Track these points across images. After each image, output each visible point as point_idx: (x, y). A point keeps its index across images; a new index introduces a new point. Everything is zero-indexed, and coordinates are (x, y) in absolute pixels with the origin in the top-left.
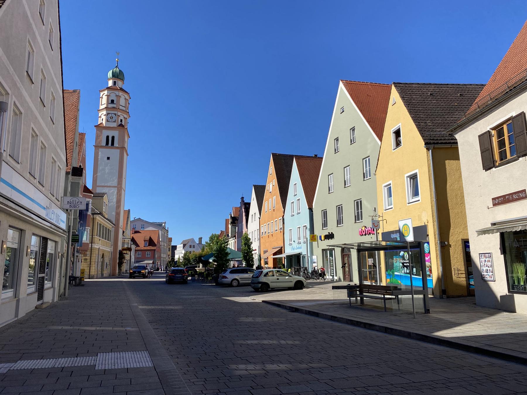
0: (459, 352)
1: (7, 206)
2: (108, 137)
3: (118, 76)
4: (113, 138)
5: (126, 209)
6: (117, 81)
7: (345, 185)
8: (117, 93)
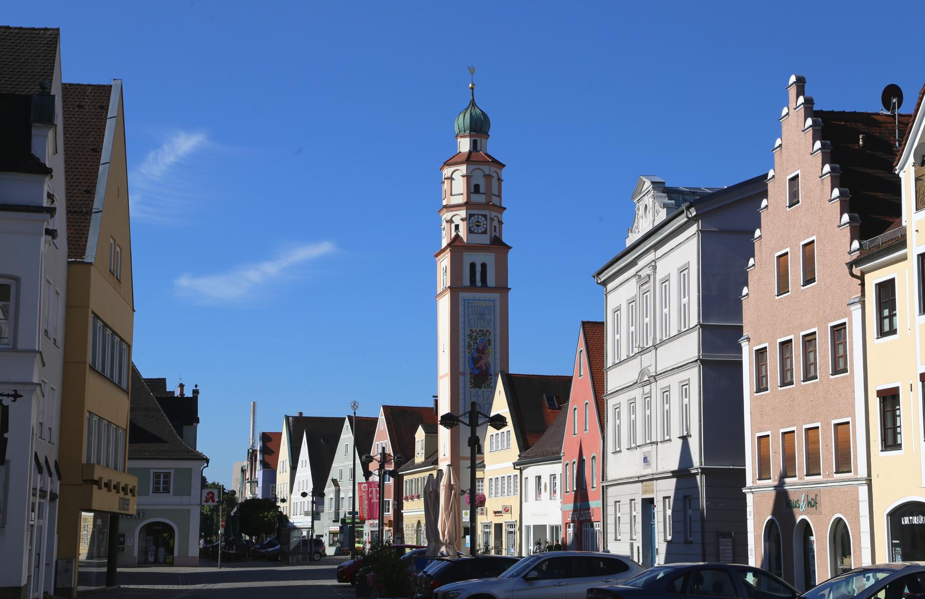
0: (662, 520)
1: (90, 434)
2: (473, 266)
3: (479, 128)
4: (484, 266)
5: (879, 383)
6: (478, 139)
7: (39, 209)
8: (486, 169)
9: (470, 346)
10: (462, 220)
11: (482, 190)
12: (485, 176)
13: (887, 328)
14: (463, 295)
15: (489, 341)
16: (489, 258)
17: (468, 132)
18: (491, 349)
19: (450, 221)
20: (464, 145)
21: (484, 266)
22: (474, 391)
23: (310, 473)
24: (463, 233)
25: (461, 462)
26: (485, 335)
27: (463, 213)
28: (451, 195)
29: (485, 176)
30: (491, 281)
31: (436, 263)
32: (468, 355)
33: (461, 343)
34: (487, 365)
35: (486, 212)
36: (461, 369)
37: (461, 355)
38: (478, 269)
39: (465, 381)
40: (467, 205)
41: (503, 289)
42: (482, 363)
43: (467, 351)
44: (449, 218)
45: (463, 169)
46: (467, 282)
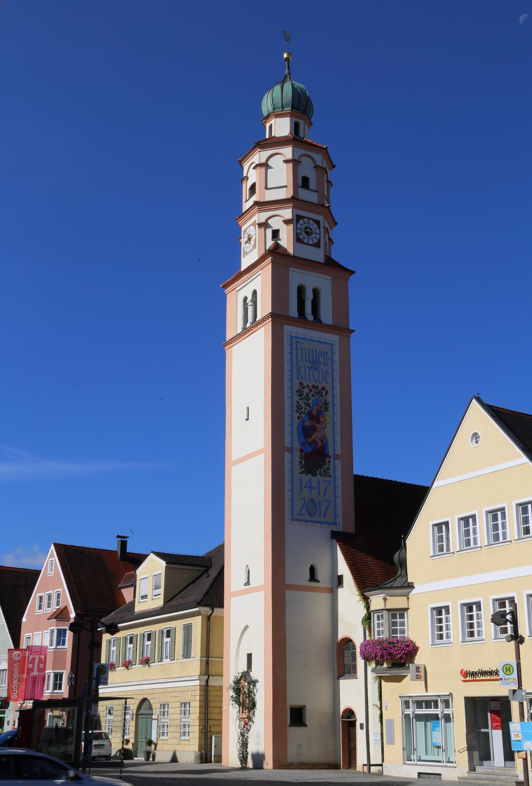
0: (161, 770)
2: (301, 290)
4: (316, 293)
6: (302, 123)
9: (299, 408)
10: (287, 222)
11: (313, 184)
12: (316, 167)
14: (289, 330)
15: (326, 404)
16: (322, 282)
17: (288, 109)
18: (328, 415)
19: (264, 225)
20: (281, 127)
21: (316, 293)
22: (306, 478)
24: (286, 241)
26: (319, 393)
27: (287, 213)
28: (266, 188)
29: (316, 167)
30: (326, 315)
31: (225, 296)
32: (296, 422)
33: (287, 402)
34: (324, 439)
36: (287, 444)
37: (287, 420)
39: (293, 461)
40: (294, 201)
41: (343, 330)
42: (316, 436)
43: (296, 415)
44: (263, 220)
45: (288, 152)
46: (294, 312)
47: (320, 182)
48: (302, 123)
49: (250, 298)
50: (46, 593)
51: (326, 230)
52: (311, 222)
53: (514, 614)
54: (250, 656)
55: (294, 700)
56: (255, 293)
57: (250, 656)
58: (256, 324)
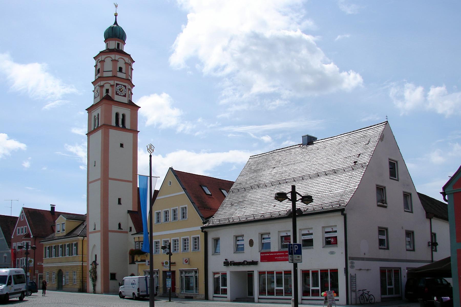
2: (117, 115)
4: (124, 116)
6: (120, 43)
11: (124, 70)
12: (126, 63)
13: (238, 239)
16: (127, 112)
21: (124, 116)
23: (100, 211)
25: (420, 89)
29: (126, 63)
35: (126, 84)
38: (121, 117)
41: (135, 131)
44: (102, 84)
46: (114, 124)
47: (127, 70)
48: (120, 43)
49: (96, 116)
50: (172, 209)
51: (129, 90)
52: (122, 86)
53: (170, 246)
54: (96, 255)
55: (112, 270)
56: (98, 114)
57: (96, 255)
58: (98, 128)
